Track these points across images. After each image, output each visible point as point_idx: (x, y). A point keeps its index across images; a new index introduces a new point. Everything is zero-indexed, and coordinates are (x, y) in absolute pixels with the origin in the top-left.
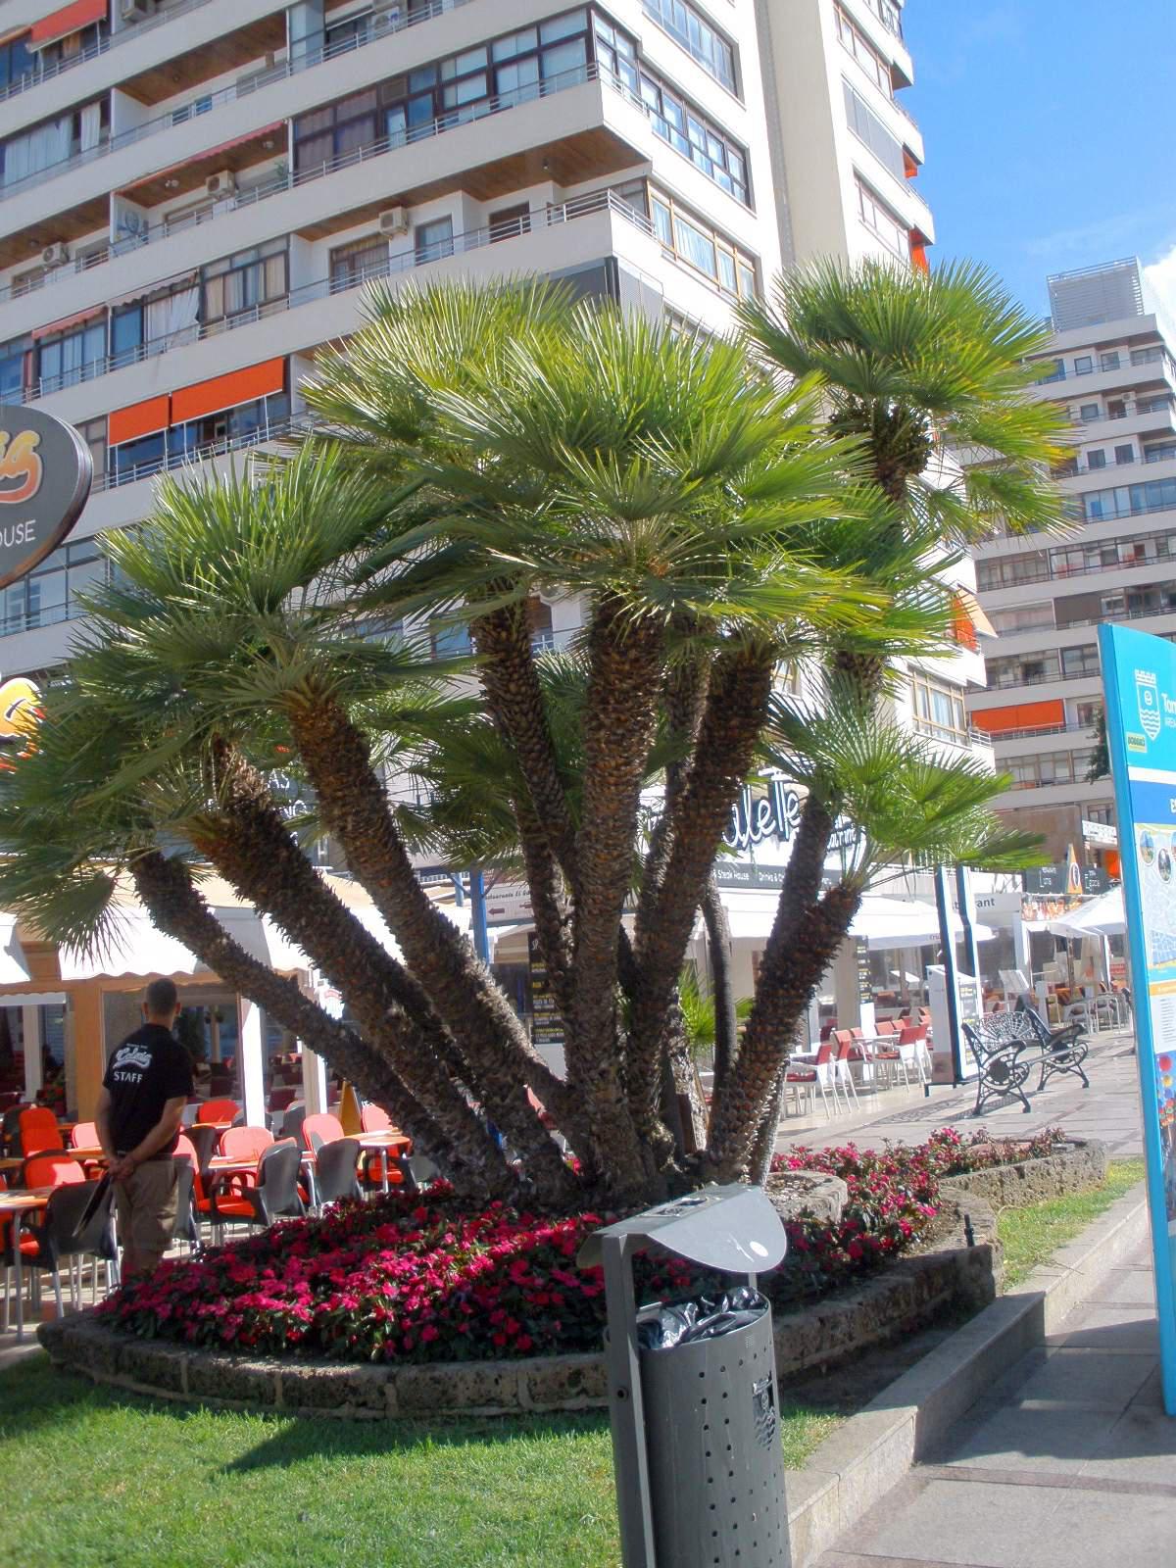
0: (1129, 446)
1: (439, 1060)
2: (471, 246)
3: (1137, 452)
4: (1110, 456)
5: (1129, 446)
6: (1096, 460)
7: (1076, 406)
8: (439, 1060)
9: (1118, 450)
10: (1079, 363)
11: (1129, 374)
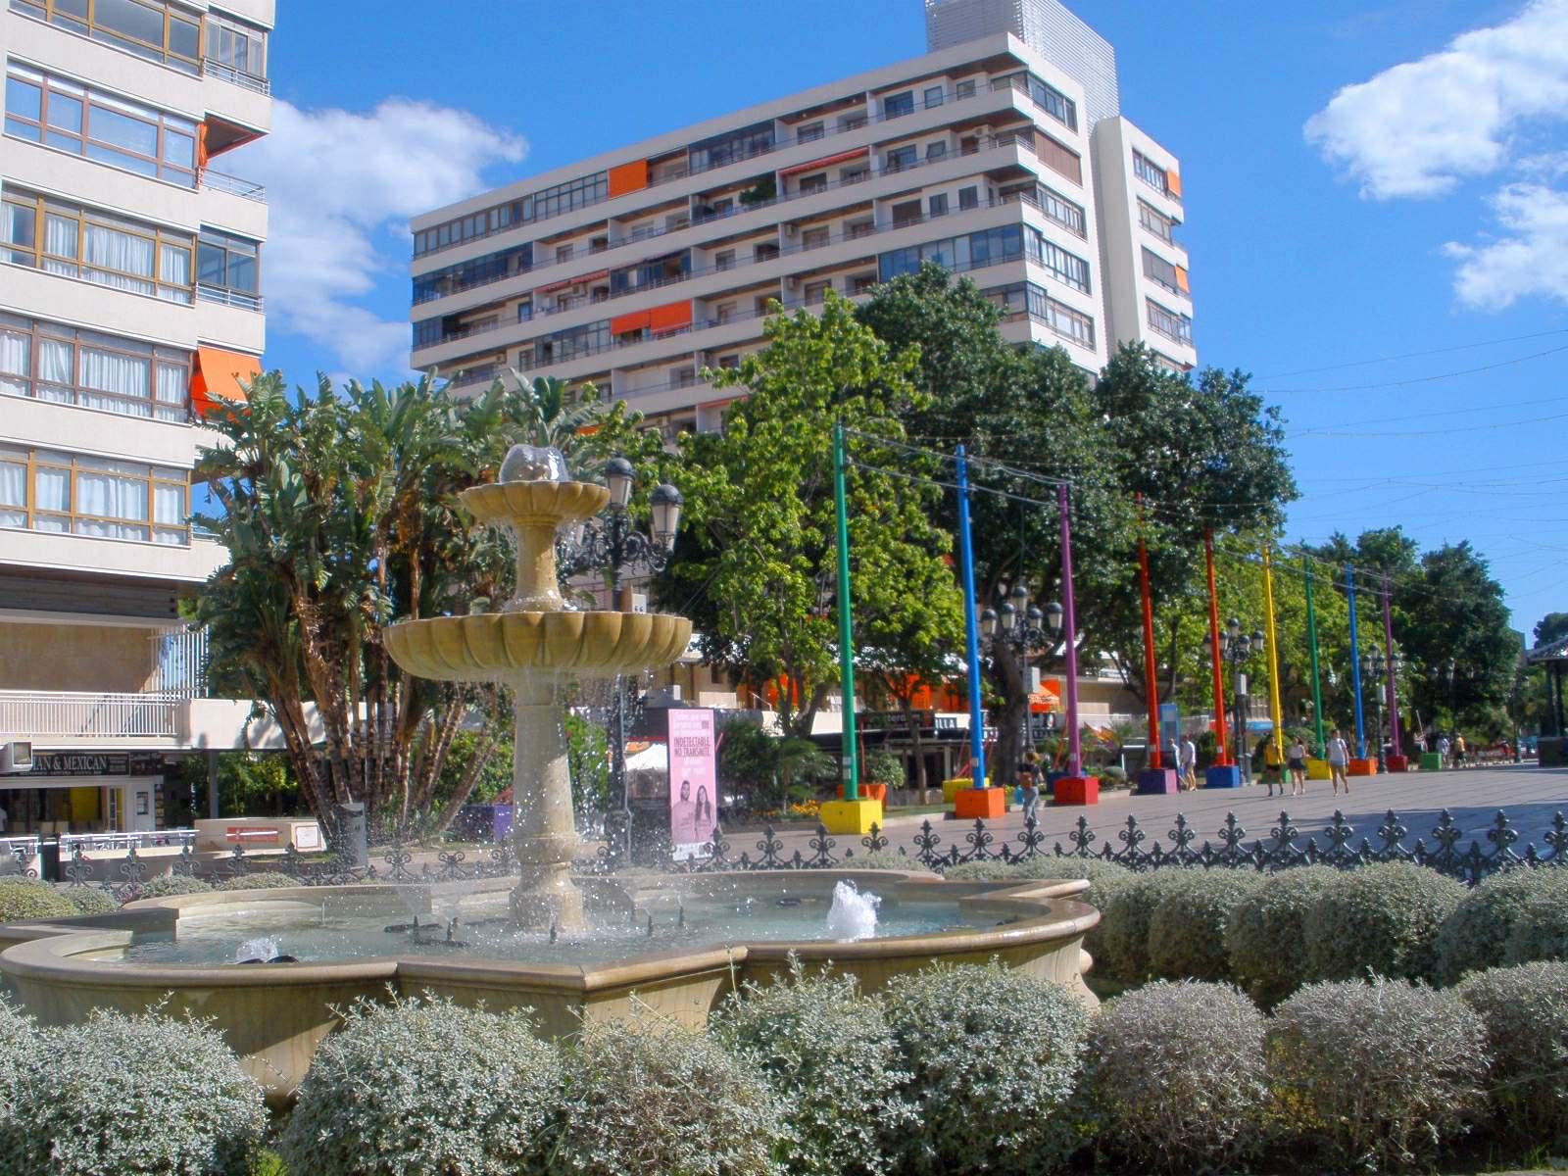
0: (974, 189)
1: (577, 711)
2: (956, 156)
3: (982, 194)
4: (953, 200)
5: (974, 189)
6: (939, 206)
7: (922, 146)
8: (577, 711)
9: (962, 193)
10: (930, 95)
11: (983, 102)
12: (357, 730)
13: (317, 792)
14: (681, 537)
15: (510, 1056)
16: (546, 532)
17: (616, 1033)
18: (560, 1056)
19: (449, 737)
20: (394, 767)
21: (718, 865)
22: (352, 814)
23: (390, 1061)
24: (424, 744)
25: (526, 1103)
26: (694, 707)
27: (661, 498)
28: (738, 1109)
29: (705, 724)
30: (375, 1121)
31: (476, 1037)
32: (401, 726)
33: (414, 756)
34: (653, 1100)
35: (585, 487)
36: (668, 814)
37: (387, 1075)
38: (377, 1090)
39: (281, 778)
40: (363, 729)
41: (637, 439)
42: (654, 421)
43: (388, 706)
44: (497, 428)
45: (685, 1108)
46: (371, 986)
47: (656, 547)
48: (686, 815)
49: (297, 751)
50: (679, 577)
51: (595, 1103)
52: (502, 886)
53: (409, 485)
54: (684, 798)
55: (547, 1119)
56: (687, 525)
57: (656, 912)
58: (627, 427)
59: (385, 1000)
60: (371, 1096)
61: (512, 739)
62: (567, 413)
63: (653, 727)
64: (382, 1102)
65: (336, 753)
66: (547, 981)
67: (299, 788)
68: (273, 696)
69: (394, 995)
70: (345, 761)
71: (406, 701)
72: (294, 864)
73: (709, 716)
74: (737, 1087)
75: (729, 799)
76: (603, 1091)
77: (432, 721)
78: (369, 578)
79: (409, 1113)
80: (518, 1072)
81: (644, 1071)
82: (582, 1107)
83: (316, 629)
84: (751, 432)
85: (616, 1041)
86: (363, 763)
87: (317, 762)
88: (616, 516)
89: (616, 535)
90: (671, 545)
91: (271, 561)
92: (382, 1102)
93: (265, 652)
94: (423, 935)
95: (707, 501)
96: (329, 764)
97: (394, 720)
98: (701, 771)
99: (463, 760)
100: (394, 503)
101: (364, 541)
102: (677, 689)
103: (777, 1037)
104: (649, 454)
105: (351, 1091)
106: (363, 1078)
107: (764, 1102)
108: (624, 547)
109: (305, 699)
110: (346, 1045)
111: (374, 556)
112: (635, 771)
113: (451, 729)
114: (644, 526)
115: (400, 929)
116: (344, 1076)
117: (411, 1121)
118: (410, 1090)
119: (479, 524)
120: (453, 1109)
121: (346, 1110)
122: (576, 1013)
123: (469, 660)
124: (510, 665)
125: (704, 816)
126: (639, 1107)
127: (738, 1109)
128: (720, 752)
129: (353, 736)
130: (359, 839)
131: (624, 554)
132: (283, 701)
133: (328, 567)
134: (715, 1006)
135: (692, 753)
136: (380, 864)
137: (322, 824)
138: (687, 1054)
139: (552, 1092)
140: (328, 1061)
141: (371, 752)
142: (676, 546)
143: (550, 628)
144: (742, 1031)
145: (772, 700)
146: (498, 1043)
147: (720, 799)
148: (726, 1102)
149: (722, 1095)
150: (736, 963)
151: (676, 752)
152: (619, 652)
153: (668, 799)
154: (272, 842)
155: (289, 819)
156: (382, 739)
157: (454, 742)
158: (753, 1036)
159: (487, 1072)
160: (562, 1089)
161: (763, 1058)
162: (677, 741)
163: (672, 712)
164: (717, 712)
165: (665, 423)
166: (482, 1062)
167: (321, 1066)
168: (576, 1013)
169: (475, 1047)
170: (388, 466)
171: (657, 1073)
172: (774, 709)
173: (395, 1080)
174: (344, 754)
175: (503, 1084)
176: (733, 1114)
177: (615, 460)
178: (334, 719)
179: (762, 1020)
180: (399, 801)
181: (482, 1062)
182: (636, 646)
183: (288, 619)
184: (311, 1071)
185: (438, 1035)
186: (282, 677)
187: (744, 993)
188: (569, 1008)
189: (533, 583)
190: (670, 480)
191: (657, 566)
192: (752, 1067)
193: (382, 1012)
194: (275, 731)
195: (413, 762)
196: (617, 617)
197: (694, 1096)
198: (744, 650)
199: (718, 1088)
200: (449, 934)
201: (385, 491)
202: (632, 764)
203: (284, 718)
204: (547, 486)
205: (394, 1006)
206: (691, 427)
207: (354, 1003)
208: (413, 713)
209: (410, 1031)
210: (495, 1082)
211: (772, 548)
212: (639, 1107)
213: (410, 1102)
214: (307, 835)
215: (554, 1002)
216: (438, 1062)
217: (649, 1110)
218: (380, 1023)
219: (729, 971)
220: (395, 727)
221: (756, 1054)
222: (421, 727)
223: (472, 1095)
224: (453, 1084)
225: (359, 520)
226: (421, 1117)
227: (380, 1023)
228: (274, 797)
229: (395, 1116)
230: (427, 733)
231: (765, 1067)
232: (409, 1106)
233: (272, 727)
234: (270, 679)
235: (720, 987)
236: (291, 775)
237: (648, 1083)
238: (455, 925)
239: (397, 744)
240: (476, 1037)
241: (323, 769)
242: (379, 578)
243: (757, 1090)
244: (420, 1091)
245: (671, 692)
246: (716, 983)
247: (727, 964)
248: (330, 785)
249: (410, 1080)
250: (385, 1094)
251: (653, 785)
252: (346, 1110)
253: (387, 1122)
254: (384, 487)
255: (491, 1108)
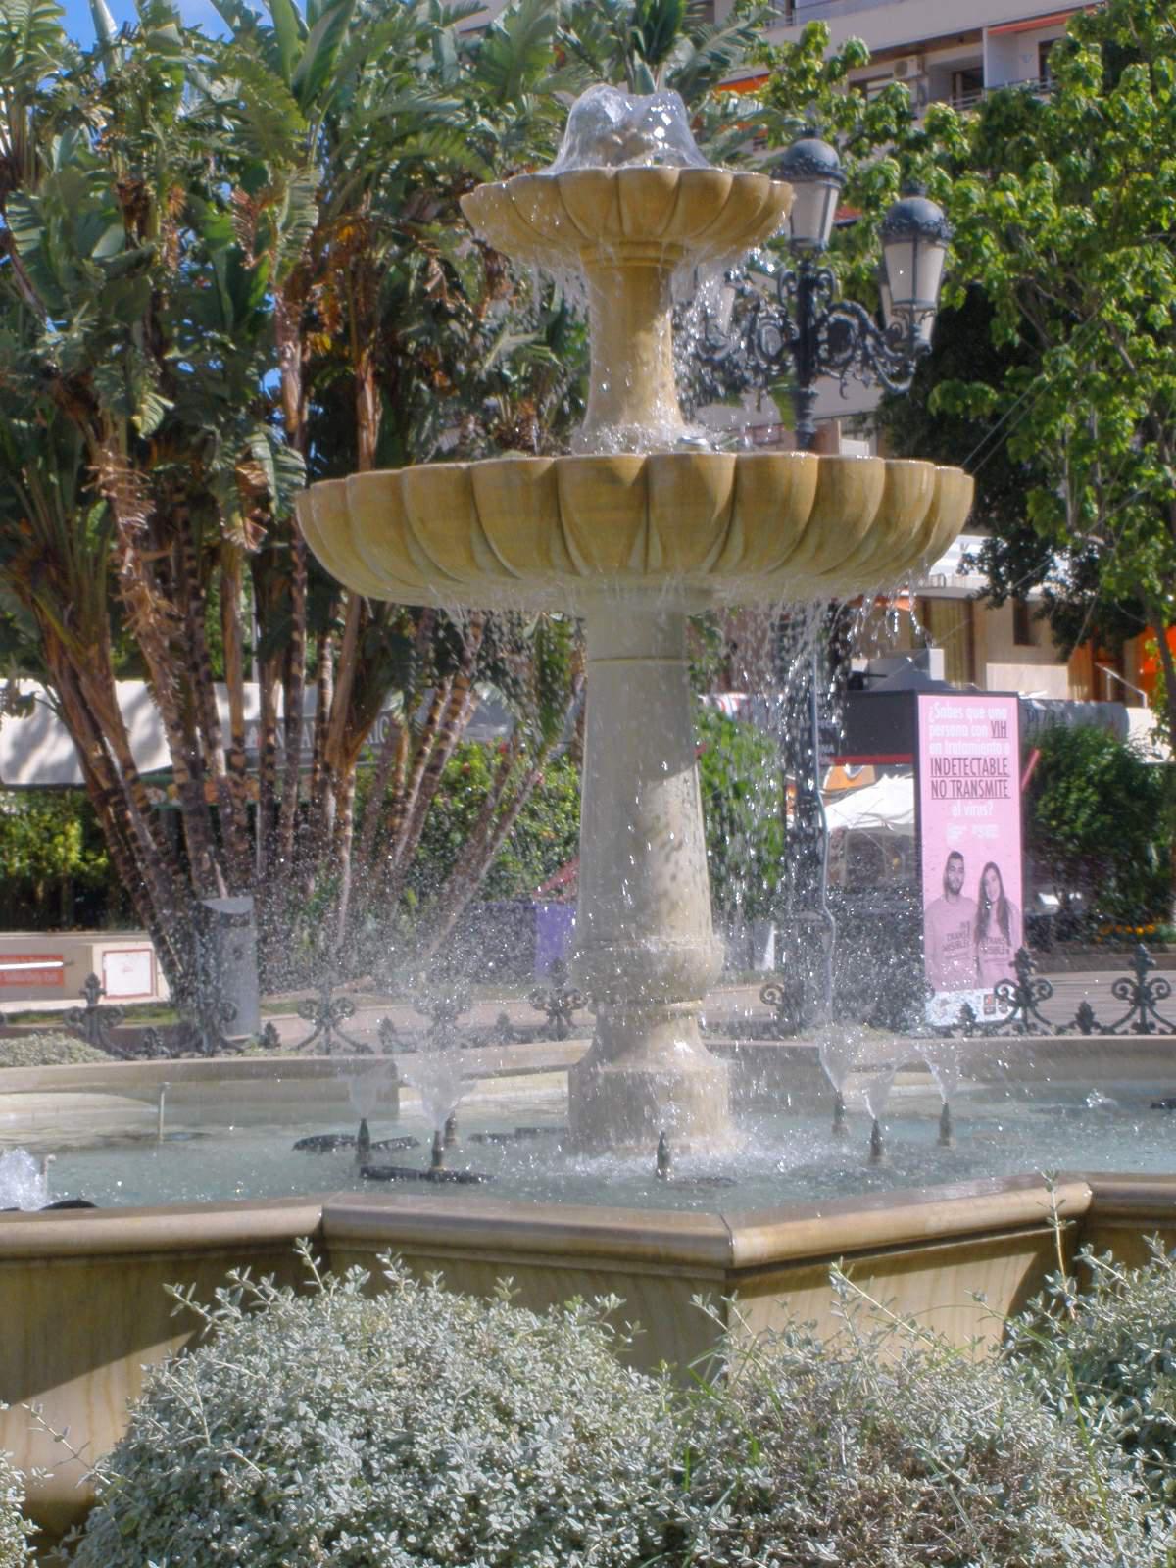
12: (239, 740)
13: (149, 875)
14: (946, 318)
15: (570, 1397)
16: (647, 284)
17: (800, 1356)
18: (675, 1405)
19: (439, 753)
20: (320, 822)
21: (1024, 1027)
22: (227, 920)
23: (303, 1408)
24: (384, 772)
25: (600, 1507)
26: (972, 692)
27: (908, 229)
28: (1068, 1535)
29: (998, 730)
30: (267, 1541)
31: (492, 1358)
32: (335, 733)
33: (364, 800)
34: (878, 1506)
35: (737, 179)
36: (917, 925)
37: (294, 1440)
38: (272, 1472)
39: (70, 848)
40: (252, 740)
41: (854, 105)
42: (888, 67)
43: (307, 691)
44: (544, 77)
45: (950, 1528)
46: (271, 1255)
47: (894, 336)
48: (954, 927)
49: (106, 785)
50: (942, 414)
51: (751, 1510)
52: (552, 1062)
53: (350, 205)
54: (952, 889)
55: (644, 1543)
56: (962, 292)
57: (890, 1117)
58: (830, 76)
59: (297, 1279)
60: (261, 1486)
61: (575, 757)
62: (698, 43)
63: (883, 732)
64: (282, 1500)
65: (192, 791)
66: (648, 1247)
67: (110, 872)
68: (54, 668)
69: (314, 1265)
70: (213, 810)
71: (346, 678)
72: (102, 1025)
73: (1006, 712)
74: (1066, 1484)
75: (1051, 901)
76: (768, 1483)
77: (400, 717)
78: (264, 410)
79: (342, 1524)
80: (585, 1439)
81: (859, 1441)
82: (721, 1518)
83: (140, 520)
84: (1111, 83)
85: (801, 1373)
86: (251, 809)
87: (152, 814)
88: (804, 269)
89: (804, 310)
90: (925, 332)
91: (48, 373)
92: (282, 1500)
93: (34, 569)
94: (378, 1160)
95: (1009, 240)
96: (177, 816)
97: (321, 718)
98: (990, 831)
99: (469, 806)
100: (316, 243)
101: (252, 329)
102: (937, 658)
103: (1156, 1377)
104: (879, 137)
105: (216, 1475)
106: (243, 1446)
107: (1127, 1523)
108: (823, 335)
109: (125, 673)
110: (206, 1376)
111: (274, 363)
112: (843, 831)
113: (444, 737)
114: (867, 288)
115: (327, 1143)
116: (201, 1443)
117: (346, 1542)
118: (345, 1473)
119: (510, 267)
120: (437, 1516)
121: (204, 1517)
122: (712, 1312)
123: (483, 559)
124: (573, 570)
125: (994, 930)
126: (848, 1521)
127: (1068, 1535)
128: (1033, 793)
129: (229, 754)
130: (240, 981)
131: (823, 352)
132: (75, 677)
133: (169, 383)
134: (1018, 1307)
135: (970, 792)
136: (293, 1029)
137: (160, 942)
138: (957, 1405)
139: (656, 1483)
140: (167, 1411)
141: (268, 787)
142: (936, 334)
143: (663, 485)
144: (1079, 1363)
145: (1146, 682)
146: (542, 1374)
147: (1031, 898)
148: (1042, 1516)
149: (1033, 1500)
150: (1064, 1217)
151: (934, 788)
152: (812, 541)
153: (916, 890)
154: (51, 984)
155: (89, 934)
156: (292, 758)
157: (451, 766)
158: (1103, 1373)
159: (514, 1436)
160: (678, 1478)
161: (1128, 1421)
162: (938, 765)
163: (924, 701)
164: (1024, 707)
165: (913, 70)
166: (504, 1414)
167: (152, 1421)
168: (712, 1312)
169: (490, 1381)
170: (302, 163)
171: (886, 1444)
172: (1152, 705)
173: (313, 1450)
174: (211, 795)
175: (551, 1463)
176: (1056, 1545)
177: (803, 143)
178: (187, 717)
179: (1123, 1338)
180: (331, 892)
181: (504, 1414)
182: (855, 524)
183: (86, 500)
184: (131, 1432)
185: (408, 1351)
186: (73, 622)
187: (1082, 1275)
188: (697, 1300)
189: (624, 399)
190: (924, 190)
191: (897, 378)
192: (1100, 1443)
193: (287, 1303)
194: (57, 749)
195: (360, 811)
196: (806, 464)
197: (970, 1501)
198: (1086, 573)
199: (1023, 1483)
200: (437, 1156)
201: (297, 202)
202: (837, 816)
203: (78, 712)
204: (652, 178)
205: (312, 1291)
206: (967, 80)
207: (228, 1283)
208: (362, 701)
209: (348, 1344)
210: (532, 1458)
211: (1151, 346)
212: (848, 1521)
213: (344, 1500)
214: (127, 969)
215: (664, 1289)
216: (407, 1412)
217: (869, 1527)
218: (284, 1327)
219: (1053, 1235)
220: (322, 735)
221: (1110, 1413)
222: (378, 733)
223: (480, 1487)
224: (440, 1462)
225: (240, 282)
226: (367, 1533)
227: (284, 1327)
228: (54, 895)
229: (311, 1530)
230: (392, 746)
231: (1130, 1443)
232: (342, 1508)
233: (51, 737)
234: (45, 632)
235: (1032, 1268)
236: (92, 839)
237: (868, 1467)
238: (448, 1141)
239: (327, 768)
240: (492, 1358)
241: (163, 825)
242: (286, 410)
243: (1112, 1495)
244: (367, 1474)
245: (923, 662)
246: (1022, 1263)
247: (1041, 1222)
248: (179, 858)
249: (346, 1452)
250: (291, 1481)
251: (885, 857)
252: (204, 1517)
253: (294, 1543)
254: (296, 206)
255: (521, 1517)
